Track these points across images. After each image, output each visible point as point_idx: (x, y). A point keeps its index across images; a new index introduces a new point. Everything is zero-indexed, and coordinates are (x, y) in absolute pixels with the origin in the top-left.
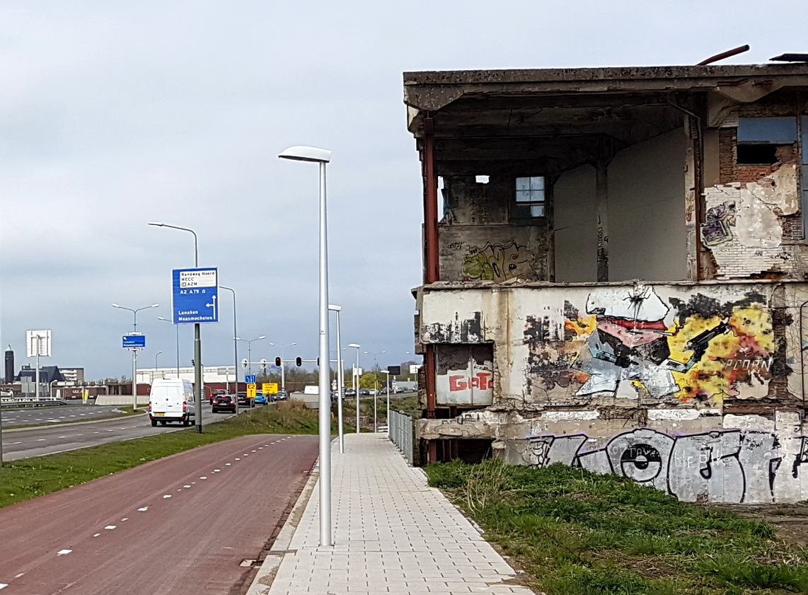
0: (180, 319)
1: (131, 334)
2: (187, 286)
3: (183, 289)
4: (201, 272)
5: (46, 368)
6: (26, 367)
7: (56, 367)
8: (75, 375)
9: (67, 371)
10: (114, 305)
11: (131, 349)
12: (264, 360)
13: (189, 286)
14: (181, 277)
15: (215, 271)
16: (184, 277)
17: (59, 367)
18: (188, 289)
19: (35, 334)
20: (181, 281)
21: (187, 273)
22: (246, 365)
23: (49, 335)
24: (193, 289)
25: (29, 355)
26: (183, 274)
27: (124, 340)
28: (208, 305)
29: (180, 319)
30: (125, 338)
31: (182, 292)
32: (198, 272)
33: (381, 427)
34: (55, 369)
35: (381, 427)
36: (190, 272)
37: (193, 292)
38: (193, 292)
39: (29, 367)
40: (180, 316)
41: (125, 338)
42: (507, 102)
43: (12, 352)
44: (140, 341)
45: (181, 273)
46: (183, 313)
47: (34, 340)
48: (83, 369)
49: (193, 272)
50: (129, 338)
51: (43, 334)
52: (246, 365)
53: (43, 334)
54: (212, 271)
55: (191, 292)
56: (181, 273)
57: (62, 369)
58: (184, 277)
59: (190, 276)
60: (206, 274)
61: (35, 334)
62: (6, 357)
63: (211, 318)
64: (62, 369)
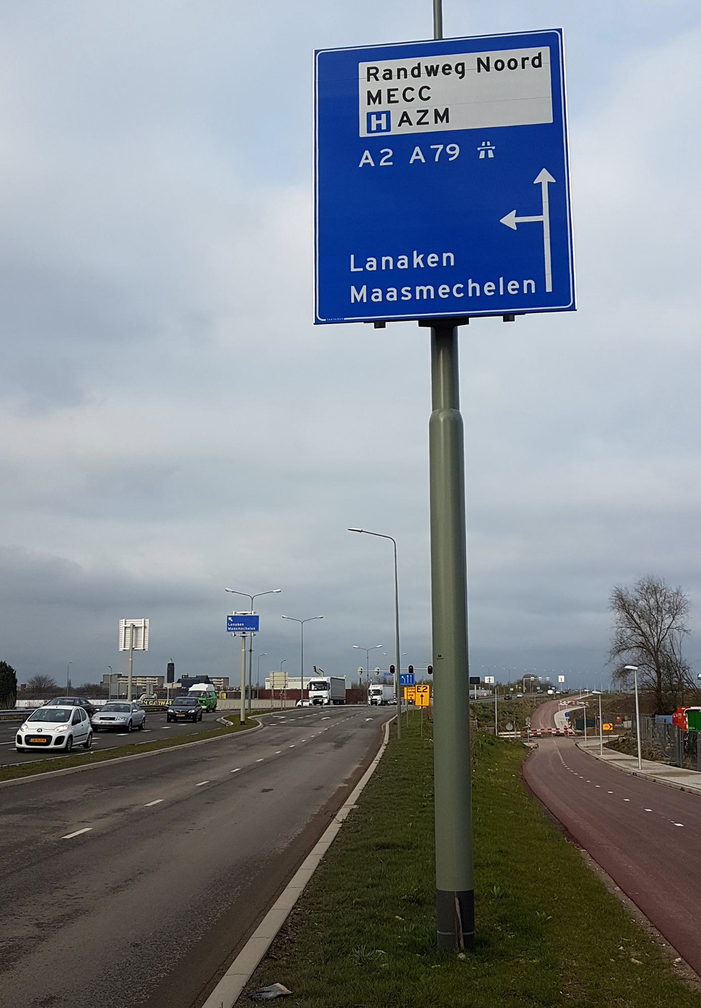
0: (357, 295)
1: (239, 613)
2: (396, 130)
3: (375, 145)
4: (469, 59)
5: (200, 676)
6: (185, 676)
7: (207, 676)
8: (222, 683)
9: (216, 680)
10: (227, 589)
11: (239, 634)
12: (378, 668)
13: (406, 129)
14: (365, 86)
15: (545, 51)
16: (383, 86)
17: (209, 677)
18: (404, 144)
19: (130, 622)
20: (364, 108)
21: (394, 65)
22: (362, 672)
23: (147, 625)
24: (425, 140)
25: (121, 649)
26: (372, 74)
27: (228, 621)
28: (510, 220)
29: (357, 295)
30: (230, 619)
31: (367, 158)
32: (452, 59)
33: (502, 733)
34: (206, 677)
35: (502, 733)
36: (409, 63)
37: (429, 154)
38: (429, 154)
39: (188, 676)
40: (359, 280)
41: (230, 619)
42: (464, 565)
43: (173, 664)
44: (251, 622)
45: (363, 67)
46: (372, 264)
47: (128, 631)
48: (228, 678)
49: (428, 61)
50: (236, 619)
51: (139, 623)
52: (362, 672)
53: (139, 623)
54: (531, 52)
55: (417, 155)
56: (363, 67)
57: (212, 678)
58: (383, 86)
59: (411, 81)
60: (500, 66)
61: (130, 622)
62: (168, 668)
63: (529, 284)
64: (212, 678)
